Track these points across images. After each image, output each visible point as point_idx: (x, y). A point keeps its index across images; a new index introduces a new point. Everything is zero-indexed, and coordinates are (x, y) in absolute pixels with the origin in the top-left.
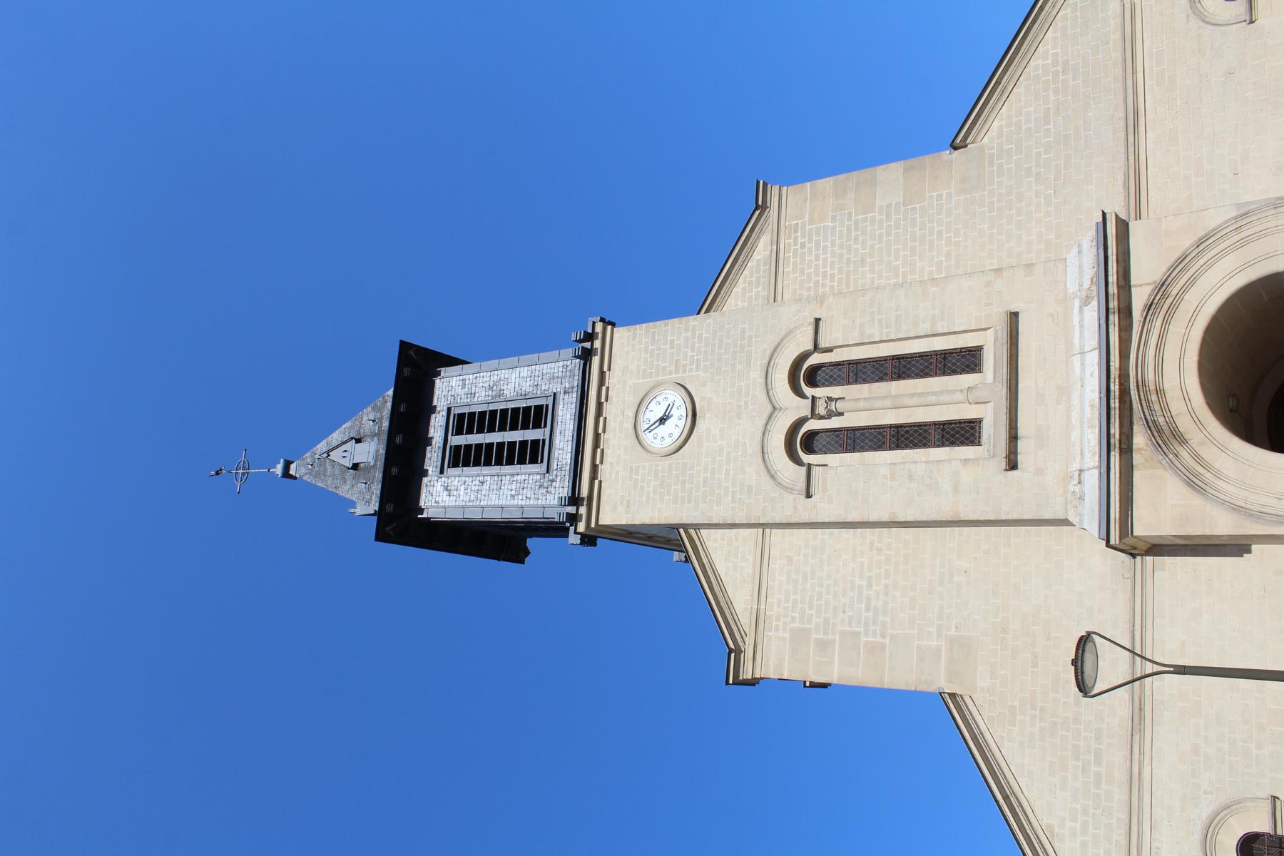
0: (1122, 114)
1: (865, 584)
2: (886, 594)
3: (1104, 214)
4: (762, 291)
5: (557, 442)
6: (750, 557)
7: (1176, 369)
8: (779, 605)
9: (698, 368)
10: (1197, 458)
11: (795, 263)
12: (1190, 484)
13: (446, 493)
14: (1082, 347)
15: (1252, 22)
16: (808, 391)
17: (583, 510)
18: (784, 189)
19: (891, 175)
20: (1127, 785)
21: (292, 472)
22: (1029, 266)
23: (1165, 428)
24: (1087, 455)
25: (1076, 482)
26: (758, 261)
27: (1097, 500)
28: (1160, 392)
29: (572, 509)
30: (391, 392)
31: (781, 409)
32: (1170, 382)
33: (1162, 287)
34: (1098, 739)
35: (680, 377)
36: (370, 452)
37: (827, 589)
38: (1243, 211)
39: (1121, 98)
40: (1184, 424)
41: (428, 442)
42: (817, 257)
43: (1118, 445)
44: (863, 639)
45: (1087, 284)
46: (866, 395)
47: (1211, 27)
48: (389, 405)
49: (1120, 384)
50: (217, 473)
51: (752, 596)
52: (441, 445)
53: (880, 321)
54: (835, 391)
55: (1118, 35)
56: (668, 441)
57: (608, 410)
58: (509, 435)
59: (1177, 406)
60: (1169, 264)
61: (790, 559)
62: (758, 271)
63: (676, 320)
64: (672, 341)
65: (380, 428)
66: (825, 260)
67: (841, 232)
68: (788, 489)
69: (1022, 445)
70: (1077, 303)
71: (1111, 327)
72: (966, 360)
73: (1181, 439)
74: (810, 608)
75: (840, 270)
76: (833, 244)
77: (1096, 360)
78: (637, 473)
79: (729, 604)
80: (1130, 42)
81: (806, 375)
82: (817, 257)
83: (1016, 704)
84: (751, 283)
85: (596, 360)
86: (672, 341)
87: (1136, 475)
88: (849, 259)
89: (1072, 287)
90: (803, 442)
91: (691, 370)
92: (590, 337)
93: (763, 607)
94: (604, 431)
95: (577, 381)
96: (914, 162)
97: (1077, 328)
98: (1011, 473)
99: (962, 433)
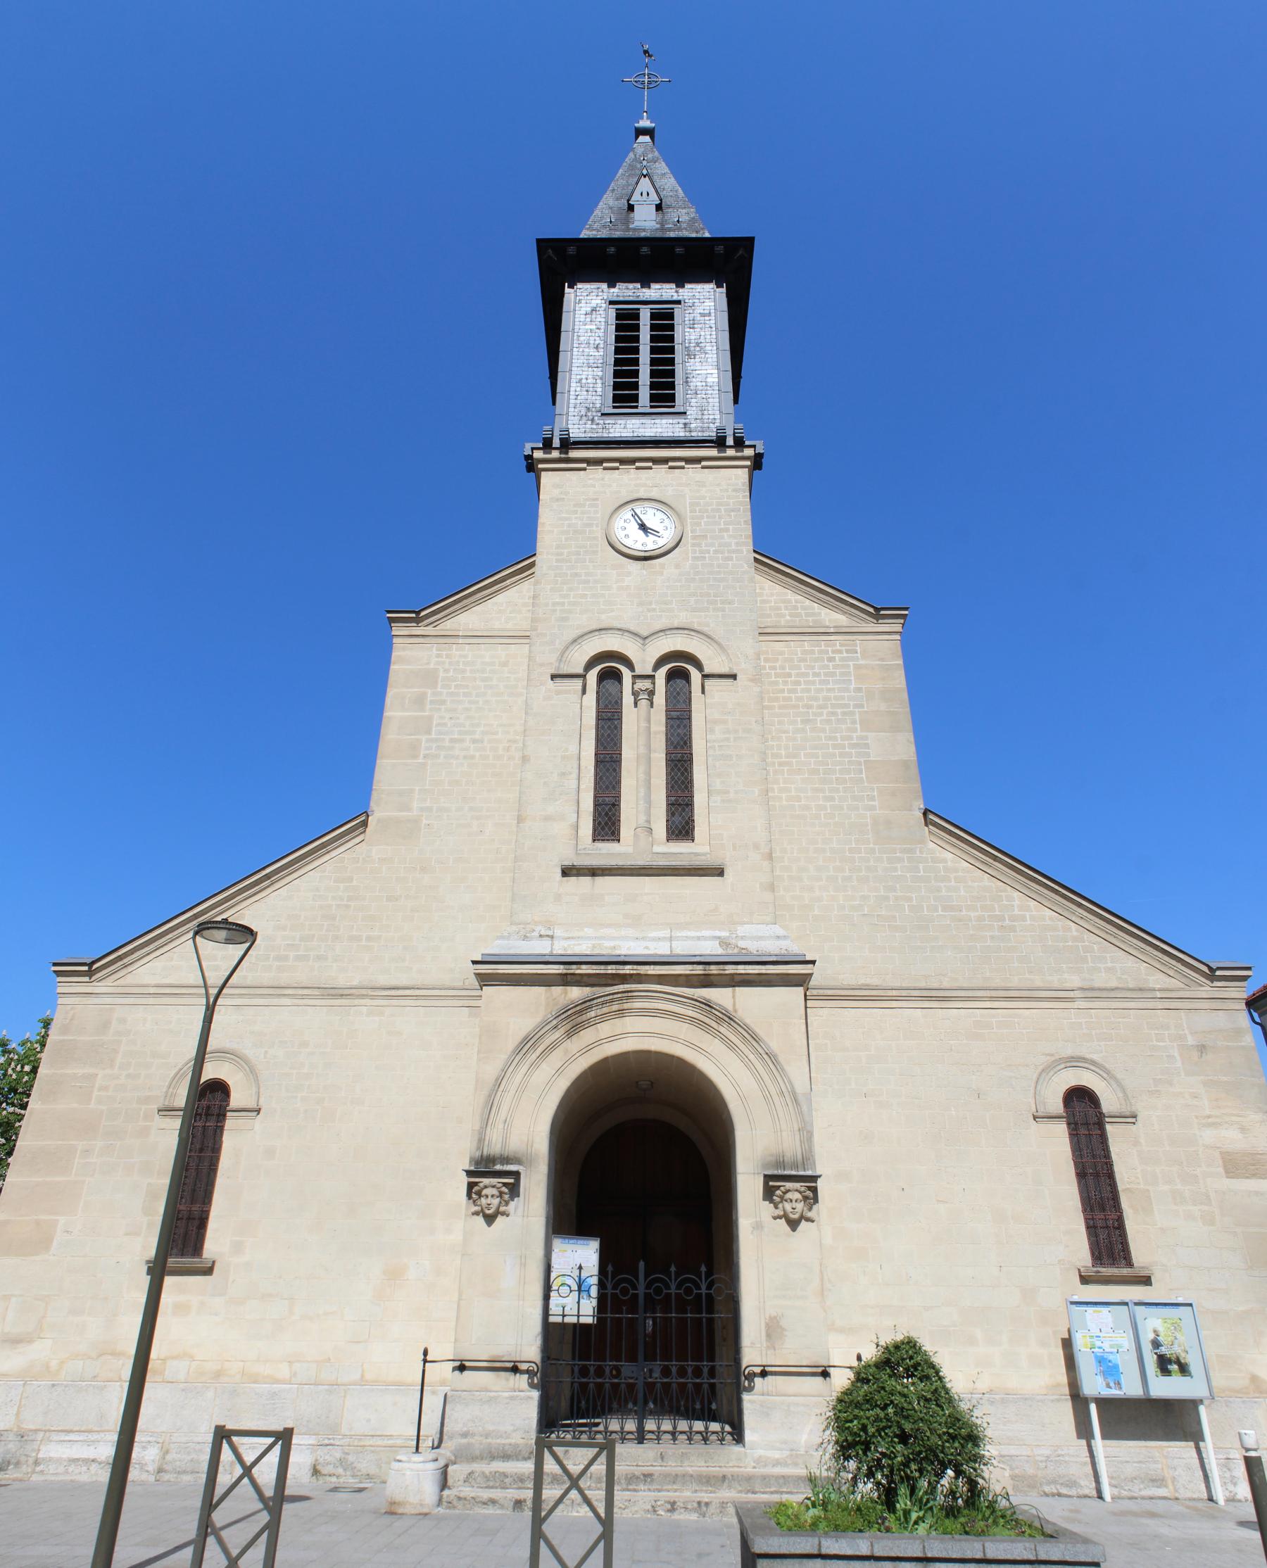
0: (946, 984)
1: (477, 737)
2: (465, 757)
3: (813, 962)
4: (785, 620)
6: (510, 626)
7: (647, 1030)
8: (461, 656)
9: (695, 558)
10: (552, 1047)
11: (812, 652)
12: (526, 1040)
13: (589, 309)
14: (678, 938)
15: (1035, 1118)
16: (663, 671)
18: (898, 637)
19: (903, 747)
20: (275, 984)
21: (642, 139)
22: (772, 888)
23: (584, 1018)
24: (565, 943)
25: (543, 933)
27: (518, 952)
28: (621, 1013)
29: (556, 443)
30: (707, 235)
33: (728, 1018)
34: (319, 958)
35: (688, 540)
36: (645, 221)
37: (476, 705)
38: (800, 1098)
39: (965, 985)
40: (587, 1036)
41: (646, 284)
43: (569, 972)
44: (424, 738)
45: (742, 944)
47: (1035, 1078)
48: (694, 235)
49: (631, 975)
50: (646, 52)
52: (642, 298)
53: (727, 739)
55: (1039, 984)
56: (620, 534)
57: (661, 470)
58: (645, 367)
59: (605, 1029)
60: (752, 1026)
61: (505, 664)
62: (807, 615)
63: (750, 532)
64: (727, 530)
65: (670, 230)
66: (813, 683)
67: (843, 698)
69: (586, 880)
70: (724, 934)
71: (690, 967)
72: (681, 827)
75: (801, 699)
76: (829, 690)
77: (660, 952)
79: (465, 608)
80: (1028, 996)
81: (679, 669)
82: (818, 675)
83: (355, 883)
84: (795, 608)
85: (714, 452)
86: (727, 530)
88: (810, 707)
89: (741, 930)
90: (609, 668)
92: (739, 443)
93: (461, 641)
94: (638, 468)
95: (696, 435)
97: (698, 934)
98: (559, 871)
99: (607, 822)
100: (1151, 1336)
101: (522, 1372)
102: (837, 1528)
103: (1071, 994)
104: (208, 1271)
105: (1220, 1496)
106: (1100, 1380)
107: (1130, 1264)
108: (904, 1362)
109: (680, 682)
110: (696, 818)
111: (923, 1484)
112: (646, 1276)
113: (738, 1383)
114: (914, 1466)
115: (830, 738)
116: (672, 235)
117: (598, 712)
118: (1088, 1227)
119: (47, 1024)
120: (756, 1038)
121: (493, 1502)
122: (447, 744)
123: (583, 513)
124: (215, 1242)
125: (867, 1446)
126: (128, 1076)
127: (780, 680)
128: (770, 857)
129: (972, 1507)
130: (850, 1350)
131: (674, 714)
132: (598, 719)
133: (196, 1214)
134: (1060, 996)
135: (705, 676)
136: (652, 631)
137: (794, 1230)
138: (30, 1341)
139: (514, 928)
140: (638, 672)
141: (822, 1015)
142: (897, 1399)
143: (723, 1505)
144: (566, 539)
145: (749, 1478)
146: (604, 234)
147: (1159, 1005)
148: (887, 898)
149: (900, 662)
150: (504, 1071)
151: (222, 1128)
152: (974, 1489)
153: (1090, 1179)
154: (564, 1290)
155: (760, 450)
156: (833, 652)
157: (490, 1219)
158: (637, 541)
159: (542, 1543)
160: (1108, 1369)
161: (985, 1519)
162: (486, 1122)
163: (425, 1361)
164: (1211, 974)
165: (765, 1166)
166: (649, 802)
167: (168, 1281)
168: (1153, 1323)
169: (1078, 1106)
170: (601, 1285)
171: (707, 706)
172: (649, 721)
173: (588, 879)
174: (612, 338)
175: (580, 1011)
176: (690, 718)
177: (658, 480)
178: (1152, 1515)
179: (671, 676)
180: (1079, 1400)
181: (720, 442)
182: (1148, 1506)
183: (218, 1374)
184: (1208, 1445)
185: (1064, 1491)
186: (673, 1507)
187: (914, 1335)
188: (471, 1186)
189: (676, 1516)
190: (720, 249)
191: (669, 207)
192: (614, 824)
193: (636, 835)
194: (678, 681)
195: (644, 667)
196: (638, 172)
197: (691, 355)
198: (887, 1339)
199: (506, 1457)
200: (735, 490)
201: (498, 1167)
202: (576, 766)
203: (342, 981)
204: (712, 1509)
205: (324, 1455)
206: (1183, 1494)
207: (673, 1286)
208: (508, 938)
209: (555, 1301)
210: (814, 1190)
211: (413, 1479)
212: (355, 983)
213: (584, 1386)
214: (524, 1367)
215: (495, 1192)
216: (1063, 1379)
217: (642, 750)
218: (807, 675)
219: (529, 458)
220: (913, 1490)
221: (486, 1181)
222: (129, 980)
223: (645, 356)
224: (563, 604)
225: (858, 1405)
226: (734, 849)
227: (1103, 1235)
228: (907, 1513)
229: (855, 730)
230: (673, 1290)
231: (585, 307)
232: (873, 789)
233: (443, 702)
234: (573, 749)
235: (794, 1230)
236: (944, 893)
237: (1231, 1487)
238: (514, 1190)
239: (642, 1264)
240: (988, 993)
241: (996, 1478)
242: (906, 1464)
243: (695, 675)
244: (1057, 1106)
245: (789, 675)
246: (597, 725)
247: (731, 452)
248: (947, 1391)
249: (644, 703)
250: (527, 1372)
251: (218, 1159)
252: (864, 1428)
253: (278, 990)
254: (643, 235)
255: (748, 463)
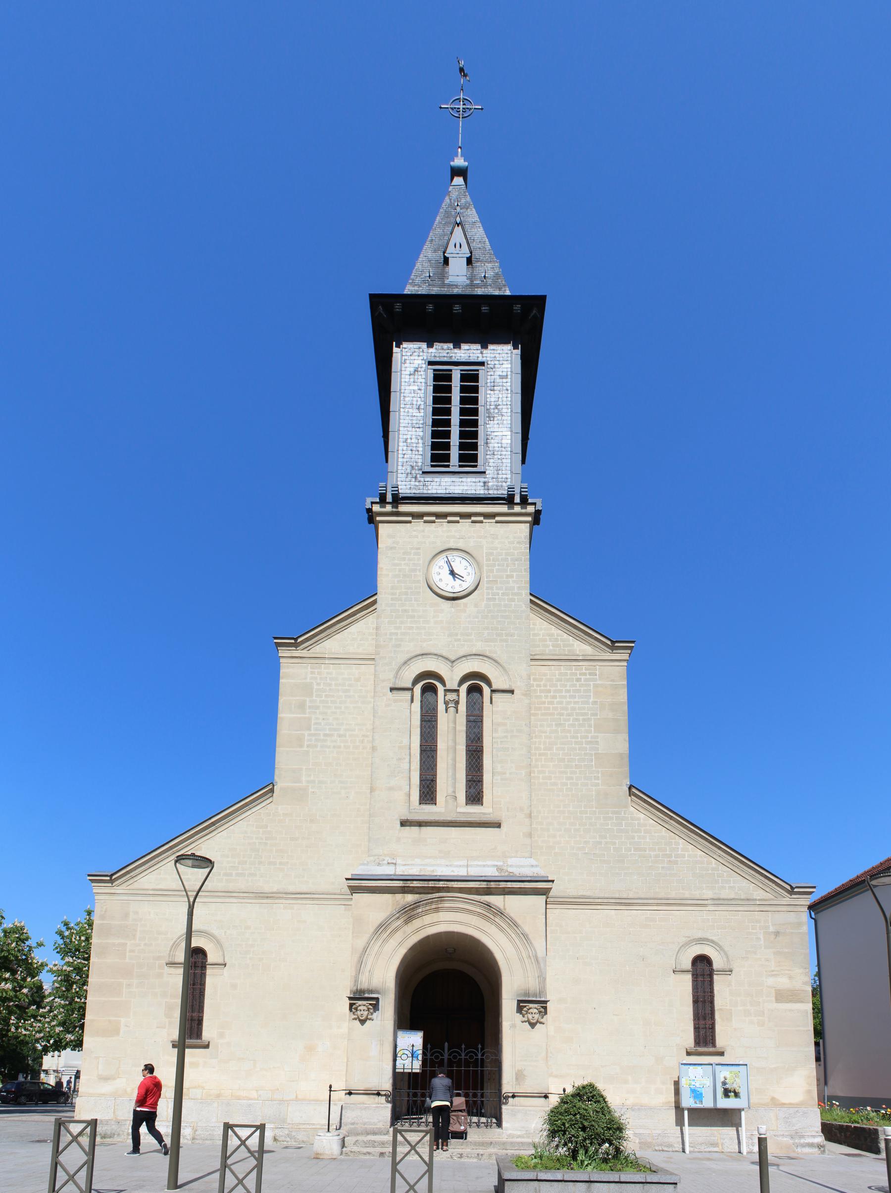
0: (631, 896)
1: (342, 732)
2: (334, 747)
3: (553, 881)
4: (549, 649)
5: (446, 480)
8: (328, 673)
10: (396, 930)
11: (566, 674)
12: (381, 926)
13: (412, 370)
14: (471, 866)
15: (674, 971)
16: (464, 689)
17: (389, 508)
18: (625, 664)
19: (620, 744)
22: (530, 835)
23: (415, 912)
24: (403, 868)
26: (573, 645)
28: (437, 910)
29: (389, 498)
30: (508, 293)
31: (452, 667)
32: (442, 916)
33: (500, 913)
35: (485, 579)
36: (458, 277)
37: (339, 702)
38: (540, 960)
40: (417, 923)
42: (568, 691)
43: (406, 885)
44: (306, 733)
45: (510, 870)
46: (458, 728)
48: (497, 293)
51: (334, 653)
52: (454, 359)
54: (462, 707)
55: (687, 895)
56: (436, 578)
57: (465, 524)
58: (455, 436)
59: (428, 919)
61: (358, 680)
64: (512, 577)
65: (478, 286)
66: (565, 697)
67: (584, 708)
68: (396, 676)
71: (479, 883)
72: (475, 795)
73: (408, 921)
74: (326, 696)
76: (575, 703)
77: (461, 874)
78: (416, 554)
79: (329, 636)
81: (476, 684)
82: (568, 691)
83: (269, 829)
84: (557, 640)
85: (504, 509)
86: (512, 577)
87: (390, 896)
88: (562, 714)
89: (510, 861)
90: (429, 684)
91: (488, 594)
93: (327, 662)
94: (449, 522)
95: (493, 493)
96: (626, 760)
98: (399, 823)
99: (428, 793)
100: (723, 1080)
101: (382, 1095)
102: (546, 1167)
103: (706, 902)
104: (207, 1046)
105: (744, 1150)
106: (692, 1100)
107: (714, 1045)
108: (588, 1094)
109: (476, 695)
110: (484, 790)
111: (592, 1149)
112: (449, 1050)
113: (500, 1101)
114: (588, 1142)
115: (573, 737)
116: (479, 292)
117: (422, 716)
118: (695, 1028)
119: (89, 913)
120: (516, 925)
121: (369, 1153)
122: (322, 737)
123: (409, 560)
124: (208, 1031)
125: (564, 1132)
126: (145, 944)
127: (543, 694)
128: (530, 816)
129: (616, 1157)
130: (560, 1085)
131: (472, 718)
132: (422, 721)
133: (196, 1018)
134: (699, 903)
135: (493, 691)
136: (458, 656)
137: (533, 1028)
138: (114, 1079)
139: (372, 858)
140: (448, 687)
141: (555, 913)
142: (582, 1111)
143: (490, 1155)
144: (398, 582)
145: (504, 1143)
146: (423, 290)
147: (757, 909)
148: (600, 843)
149: (625, 683)
150: (369, 943)
151: (205, 974)
152: (618, 1150)
153: (700, 1004)
154: (404, 1057)
155: (539, 507)
156: (580, 674)
157: (363, 1022)
158: (449, 585)
159: (397, 1174)
160: (697, 1094)
161: (622, 1164)
162: (359, 971)
163: (330, 1091)
164: (792, 891)
165: (518, 995)
166: (454, 779)
167: (187, 1050)
168: (724, 1073)
169: (699, 965)
170: (424, 1054)
171: (495, 712)
172: (455, 723)
173: (417, 828)
174: (430, 400)
175: (413, 908)
176: (482, 721)
177: (462, 533)
178: (709, 1159)
179: (470, 690)
180: (679, 1109)
181: (509, 500)
182: (708, 1155)
183: (218, 1096)
184: (743, 1130)
185: (666, 1149)
186: (461, 1156)
187: (593, 1082)
188: (351, 1005)
189: (462, 1160)
190: (517, 308)
191: (478, 260)
192: (432, 793)
193: (446, 801)
194: (475, 694)
195: (452, 684)
196: (452, 220)
197: (491, 417)
198: (579, 1083)
199: (375, 1133)
200: (518, 543)
201: (366, 995)
202: (408, 753)
203: (267, 889)
204: (484, 1157)
205: (278, 1132)
206: (726, 1150)
207: (463, 1055)
208: (367, 864)
209: (399, 1063)
210: (545, 1008)
211: (328, 1143)
212: (275, 890)
213: (415, 1102)
214: (383, 1093)
215: (365, 1008)
216: (672, 1098)
217: (451, 743)
218: (561, 691)
219: (369, 511)
220: (586, 1152)
221: (360, 1002)
222: (136, 885)
223: (455, 418)
224: (397, 634)
225: (561, 1114)
226: (508, 811)
227: (702, 1032)
228: (582, 1162)
229: (591, 732)
230: (463, 1057)
231: (409, 368)
232: (598, 772)
233: (318, 708)
234: (406, 741)
235: (533, 1028)
236: (636, 839)
237: (751, 1147)
238: (376, 1007)
239: (446, 1044)
240: (656, 901)
241: (631, 1145)
242: (585, 1140)
243: (486, 690)
244: (688, 965)
245: (549, 691)
246: (421, 725)
247: (389, 508)
248: (608, 1108)
249: (452, 710)
250: (385, 1095)
251: (204, 989)
252: (564, 1124)
253: (228, 893)
254: (456, 291)
255: (530, 519)
